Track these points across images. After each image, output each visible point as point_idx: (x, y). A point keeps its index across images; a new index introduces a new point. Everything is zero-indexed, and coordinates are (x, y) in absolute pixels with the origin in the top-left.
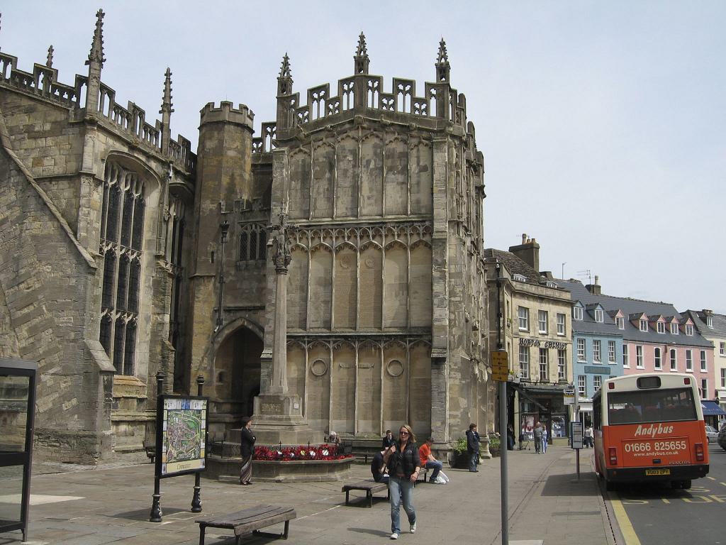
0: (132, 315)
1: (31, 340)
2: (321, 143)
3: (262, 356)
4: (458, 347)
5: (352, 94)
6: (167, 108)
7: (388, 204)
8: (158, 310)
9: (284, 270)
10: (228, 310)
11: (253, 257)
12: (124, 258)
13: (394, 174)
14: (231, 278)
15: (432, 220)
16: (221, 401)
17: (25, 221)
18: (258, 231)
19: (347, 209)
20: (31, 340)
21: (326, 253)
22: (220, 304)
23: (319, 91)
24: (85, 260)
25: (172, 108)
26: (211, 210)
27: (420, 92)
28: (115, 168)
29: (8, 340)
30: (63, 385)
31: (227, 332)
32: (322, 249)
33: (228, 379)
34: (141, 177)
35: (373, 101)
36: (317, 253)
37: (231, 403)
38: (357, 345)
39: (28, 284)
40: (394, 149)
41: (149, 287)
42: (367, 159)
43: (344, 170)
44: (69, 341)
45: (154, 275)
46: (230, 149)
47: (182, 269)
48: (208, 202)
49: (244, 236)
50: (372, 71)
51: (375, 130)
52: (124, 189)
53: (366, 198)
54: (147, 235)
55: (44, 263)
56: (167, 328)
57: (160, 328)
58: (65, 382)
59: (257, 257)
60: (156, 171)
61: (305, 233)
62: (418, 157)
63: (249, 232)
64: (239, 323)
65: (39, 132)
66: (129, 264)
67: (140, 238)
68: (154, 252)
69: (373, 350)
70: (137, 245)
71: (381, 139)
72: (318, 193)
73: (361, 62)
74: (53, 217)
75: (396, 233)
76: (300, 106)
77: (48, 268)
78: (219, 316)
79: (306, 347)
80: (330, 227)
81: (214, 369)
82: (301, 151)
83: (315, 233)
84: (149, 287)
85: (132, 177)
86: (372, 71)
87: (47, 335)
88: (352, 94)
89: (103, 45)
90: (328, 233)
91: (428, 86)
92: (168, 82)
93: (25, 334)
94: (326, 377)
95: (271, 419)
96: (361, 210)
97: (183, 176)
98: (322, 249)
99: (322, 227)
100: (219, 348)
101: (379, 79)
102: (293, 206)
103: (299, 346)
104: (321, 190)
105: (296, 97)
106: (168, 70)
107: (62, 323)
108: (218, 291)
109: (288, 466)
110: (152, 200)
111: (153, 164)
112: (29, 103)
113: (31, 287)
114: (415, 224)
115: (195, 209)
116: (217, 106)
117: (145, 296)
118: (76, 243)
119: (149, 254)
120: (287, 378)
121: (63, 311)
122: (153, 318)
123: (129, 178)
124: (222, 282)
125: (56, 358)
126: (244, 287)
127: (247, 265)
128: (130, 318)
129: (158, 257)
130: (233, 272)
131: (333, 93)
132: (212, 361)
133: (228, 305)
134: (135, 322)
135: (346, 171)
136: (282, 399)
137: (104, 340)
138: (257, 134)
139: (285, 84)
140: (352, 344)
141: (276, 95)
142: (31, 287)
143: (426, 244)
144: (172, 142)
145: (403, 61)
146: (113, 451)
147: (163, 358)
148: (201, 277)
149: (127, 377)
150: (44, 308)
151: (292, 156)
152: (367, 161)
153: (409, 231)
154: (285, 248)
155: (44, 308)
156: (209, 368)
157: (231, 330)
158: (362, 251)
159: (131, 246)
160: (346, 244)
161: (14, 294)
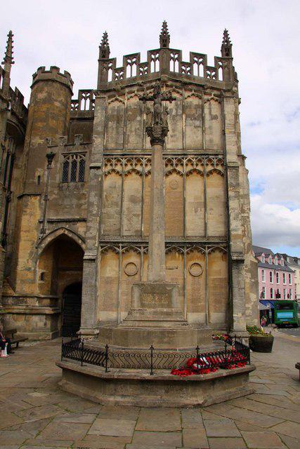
2: (133, 95)
3: (85, 258)
4: (248, 253)
5: (157, 62)
7: (187, 142)
10: (51, 222)
11: (73, 179)
14: (54, 196)
15: (224, 154)
16: (43, 296)
18: (79, 160)
21: (138, 176)
22: (44, 216)
23: (132, 58)
25: (13, 61)
27: (211, 63)
31: (49, 239)
33: (48, 278)
35: (174, 67)
37: (50, 299)
40: (191, 102)
46: (56, 101)
47: (11, 192)
49: (66, 164)
50: (171, 46)
51: (176, 87)
59: (77, 179)
61: (120, 161)
62: (210, 109)
63: (70, 161)
64: (61, 232)
71: (181, 95)
72: (131, 132)
73: (165, 38)
75: (195, 163)
76: (117, 67)
81: (37, 269)
82: (117, 100)
83: (129, 161)
86: (171, 46)
88: (157, 62)
90: (139, 161)
91: (217, 59)
92: (10, 41)
97: (17, 117)
101: (178, 52)
104: (133, 129)
105: (114, 61)
106: (11, 32)
108: (43, 207)
114: (210, 157)
115: (26, 145)
124: (46, 200)
126: (65, 203)
127: (68, 186)
130: (56, 192)
131: (144, 59)
132: (36, 263)
133: (51, 218)
138: (75, 97)
139: (104, 51)
141: (98, 58)
143: (219, 173)
145: (195, 40)
148: (28, 195)
153: (205, 161)
156: (33, 269)
157: (53, 238)
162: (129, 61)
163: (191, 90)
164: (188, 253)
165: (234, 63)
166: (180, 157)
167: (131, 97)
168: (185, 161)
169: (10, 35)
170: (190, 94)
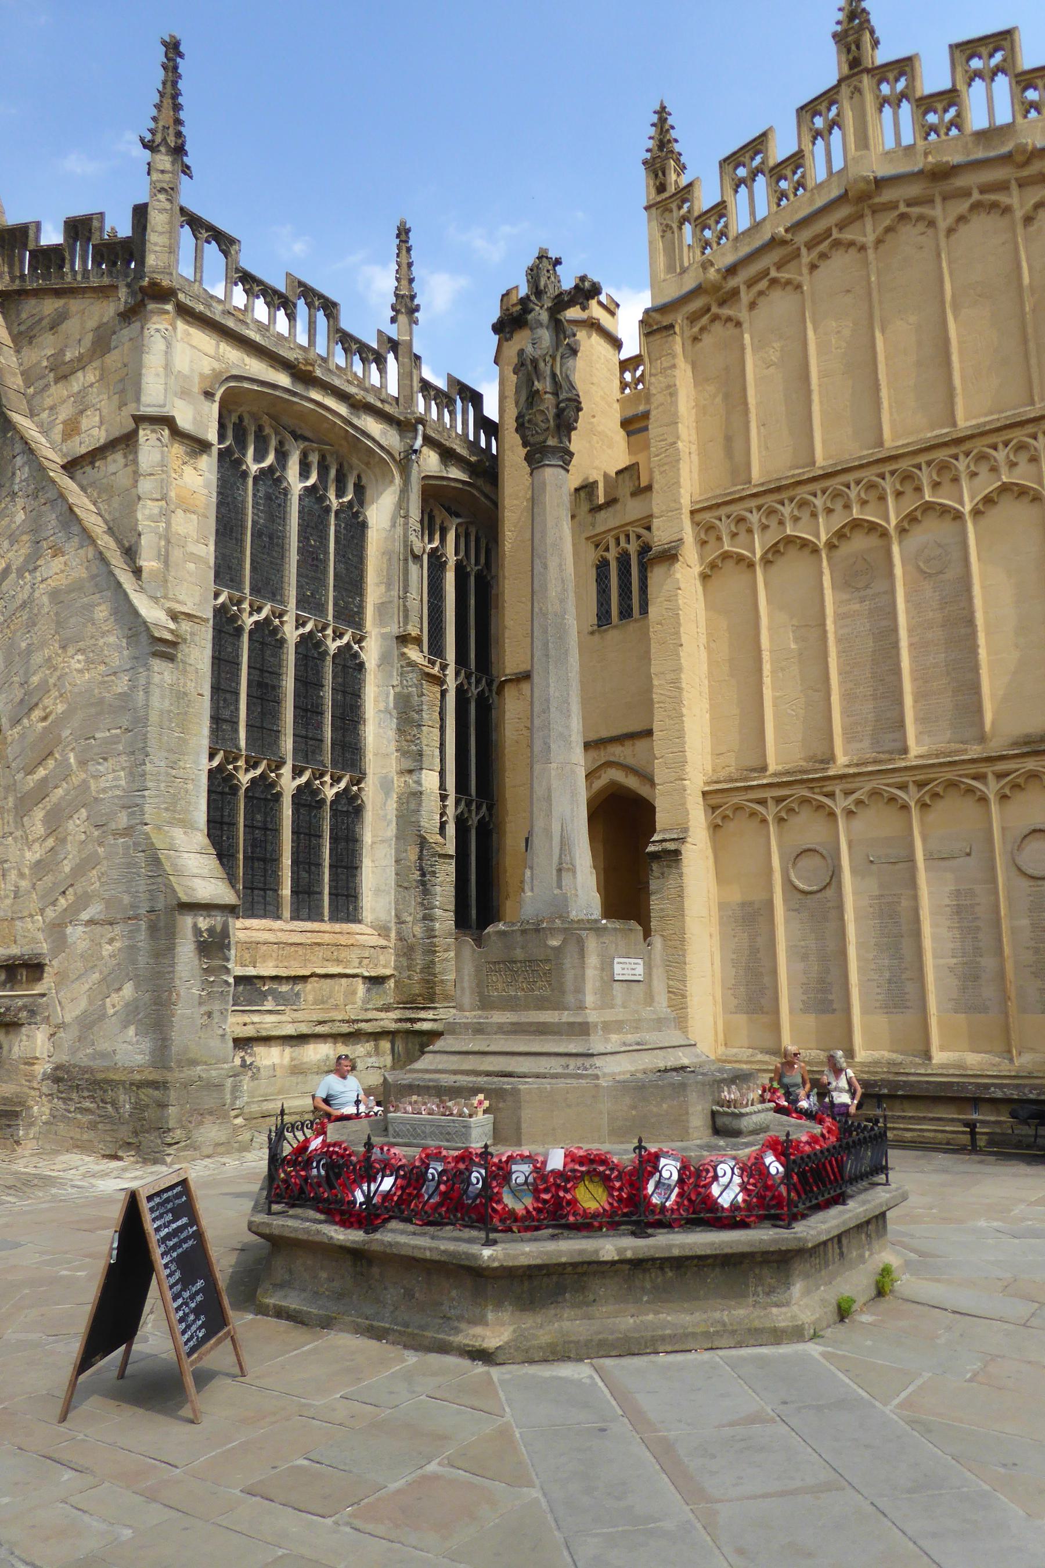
1: (50, 842)
8: (409, 764)
9: (554, 450)
12: (310, 648)
17: (39, 563)
18: (633, 548)
20: (50, 842)
23: (746, 159)
24: (145, 622)
28: (268, 430)
29: (12, 849)
30: (107, 949)
34: (344, 463)
39: (44, 709)
41: (387, 711)
44: (117, 834)
45: (395, 683)
52: (295, 483)
54: (374, 593)
55: (71, 651)
57: (413, 806)
58: (111, 941)
60: (383, 442)
63: (612, 556)
65: (72, 360)
66: (329, 660)
67: (362, 601)
68: (394, 629)
70: (351, 615)
74: (87, 537)
77: (77, 662)
82: (716, 318)
84: (387, 711)
87: (77, 825)
89: (182, 115)
93: (39, 829)
94: (829, 893)
95: (517, 1029)
107: (104, 790)
110: (381, 513)
111: (372, 426)
112: (56, 306)
113: (51, 713)
117: (377, 733)
118: (126, 579)
119: (384, 636)
121: (105, 759)
122: (398, 783)
123: (314, 458)
125: (93, 882)
128: (343, 785)
129: (403, 639)
134: (356, 796)
137: (219, 828)
142: (51, 713)
146: (239, 1121)
147: (423, 875)
149: (337, 927)
150: (72, 760)
154: (554, 375)
155: (72, 760)
159: (330, 618)
161: (23, 736)
162: (742, 172)
163: (966, 193)
164: (1004, 797)
165: (434, 1355)
166: (941, 454)
167: (761, 293)
168: (962, 465)
169: (173, 48)
170: (962, 207)
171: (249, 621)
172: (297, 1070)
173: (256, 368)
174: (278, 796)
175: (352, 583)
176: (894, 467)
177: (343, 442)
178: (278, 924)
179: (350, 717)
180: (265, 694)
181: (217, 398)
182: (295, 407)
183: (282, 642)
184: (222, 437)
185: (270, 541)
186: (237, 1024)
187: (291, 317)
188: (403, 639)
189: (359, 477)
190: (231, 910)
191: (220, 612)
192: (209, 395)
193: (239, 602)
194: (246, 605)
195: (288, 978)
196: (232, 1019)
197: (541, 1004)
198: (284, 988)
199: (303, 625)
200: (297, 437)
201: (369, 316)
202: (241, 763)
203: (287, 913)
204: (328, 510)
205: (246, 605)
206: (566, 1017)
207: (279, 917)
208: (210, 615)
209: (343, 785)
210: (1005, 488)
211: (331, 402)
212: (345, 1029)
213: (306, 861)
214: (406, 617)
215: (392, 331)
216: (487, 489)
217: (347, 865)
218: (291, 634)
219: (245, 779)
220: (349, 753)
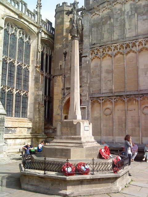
0: (25, 92)
6: (39, 6)
8: (37, 90)
12: (20, 67)
13: (141, 16)
19: (118, 36)
26: (60, 48)
32: (107, 56)
34: (27, 32)
36: (105, 58)
38: (126, 100)
42: (127, 11)
43: (116, 18)
48: (59, 44)
53: (127, 29)
56: (41, 97)
57: (38, 97)
69: (134, 102)
70: (27, 62)
72: (105, 31)
78: (64, 92)
79: (101, 102)
80: (110, 45)
81: (63, 114)
85: (23, 32)
94: (111, 116)
95: (67, 139)
96: (125, 35)
98: (107, 56)
99: (107, 46)
100: (65, 105)
102: (93, 39)
103: (98, 102)
108: (63, 81)
109: (74, 181)
116: (61, 5)
117: (31, 83)
120: (92, 117)
123: (21, 32)
124: (65, 77)
135: (117, 19)
136: (75, 124)
140: (124, 99)
144: (42, 20)
151: (92, 17)
152: (127, 12)
156: (60, 114)
158: (127, 54)
160: (119, 52)
171: (8, 62)
172: (15, 144)
173: (12, 14)
174: (13, 94)
175: (28, 56)
176: (132, 42)
177: (27, 30)
178: (12, 118)
179: (26, 80)
180: (11, 75)
181: (4, 19)
182: (19, 23)
183: (14, 66)
184: (5, 27)
185: (13, 47)
186: (5, 136)
187: (18, 6)
188: (36, 67)
189: (29, 36)
190: (5, 115)
191: (4, 59)
192: (3, 18)
193: (7, 58)
194: (8, 59)
195: (14, 128)
196: (5, 135)
197: (72, 134)
198: (13, 129)
199: (18, 63)
200: (19, 28)
201: (32, 7)
202: (6, 88)
203: (14, 116)
204: (24, 42)
205: (8, 59)
206: (77, 136)
207: (12, 116)
208: (2, 60)
209: (25, 93)
210: (144, 48)
211: (25, 22)
212: (24, 137)
213: (17, 106)
214: (37, 63)
215: (36, 10)
216: (52, 40)
217: (25, 107)
218: (16, 65)
219: (7, 91)
220: (26, 87)
